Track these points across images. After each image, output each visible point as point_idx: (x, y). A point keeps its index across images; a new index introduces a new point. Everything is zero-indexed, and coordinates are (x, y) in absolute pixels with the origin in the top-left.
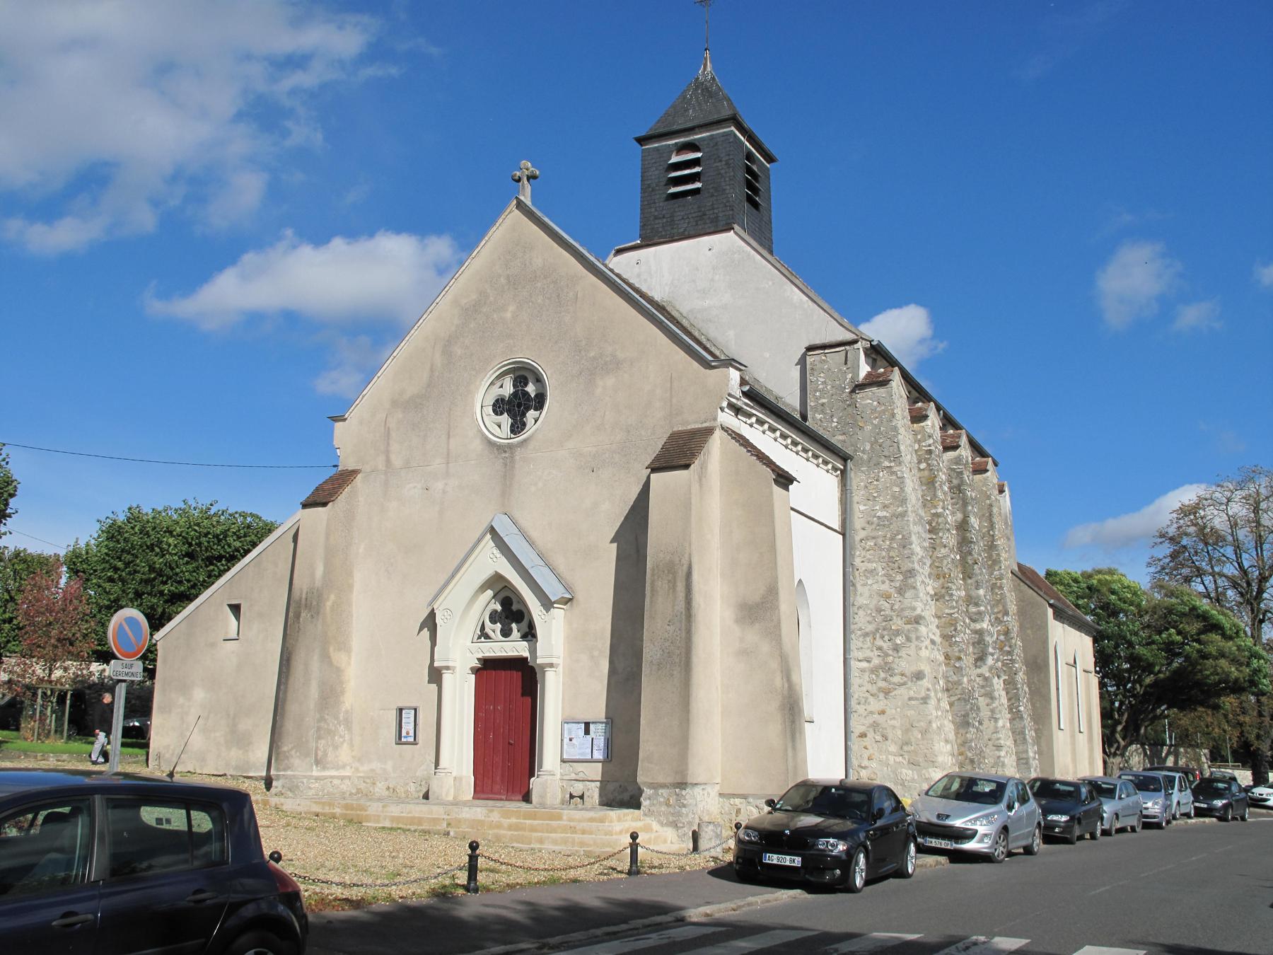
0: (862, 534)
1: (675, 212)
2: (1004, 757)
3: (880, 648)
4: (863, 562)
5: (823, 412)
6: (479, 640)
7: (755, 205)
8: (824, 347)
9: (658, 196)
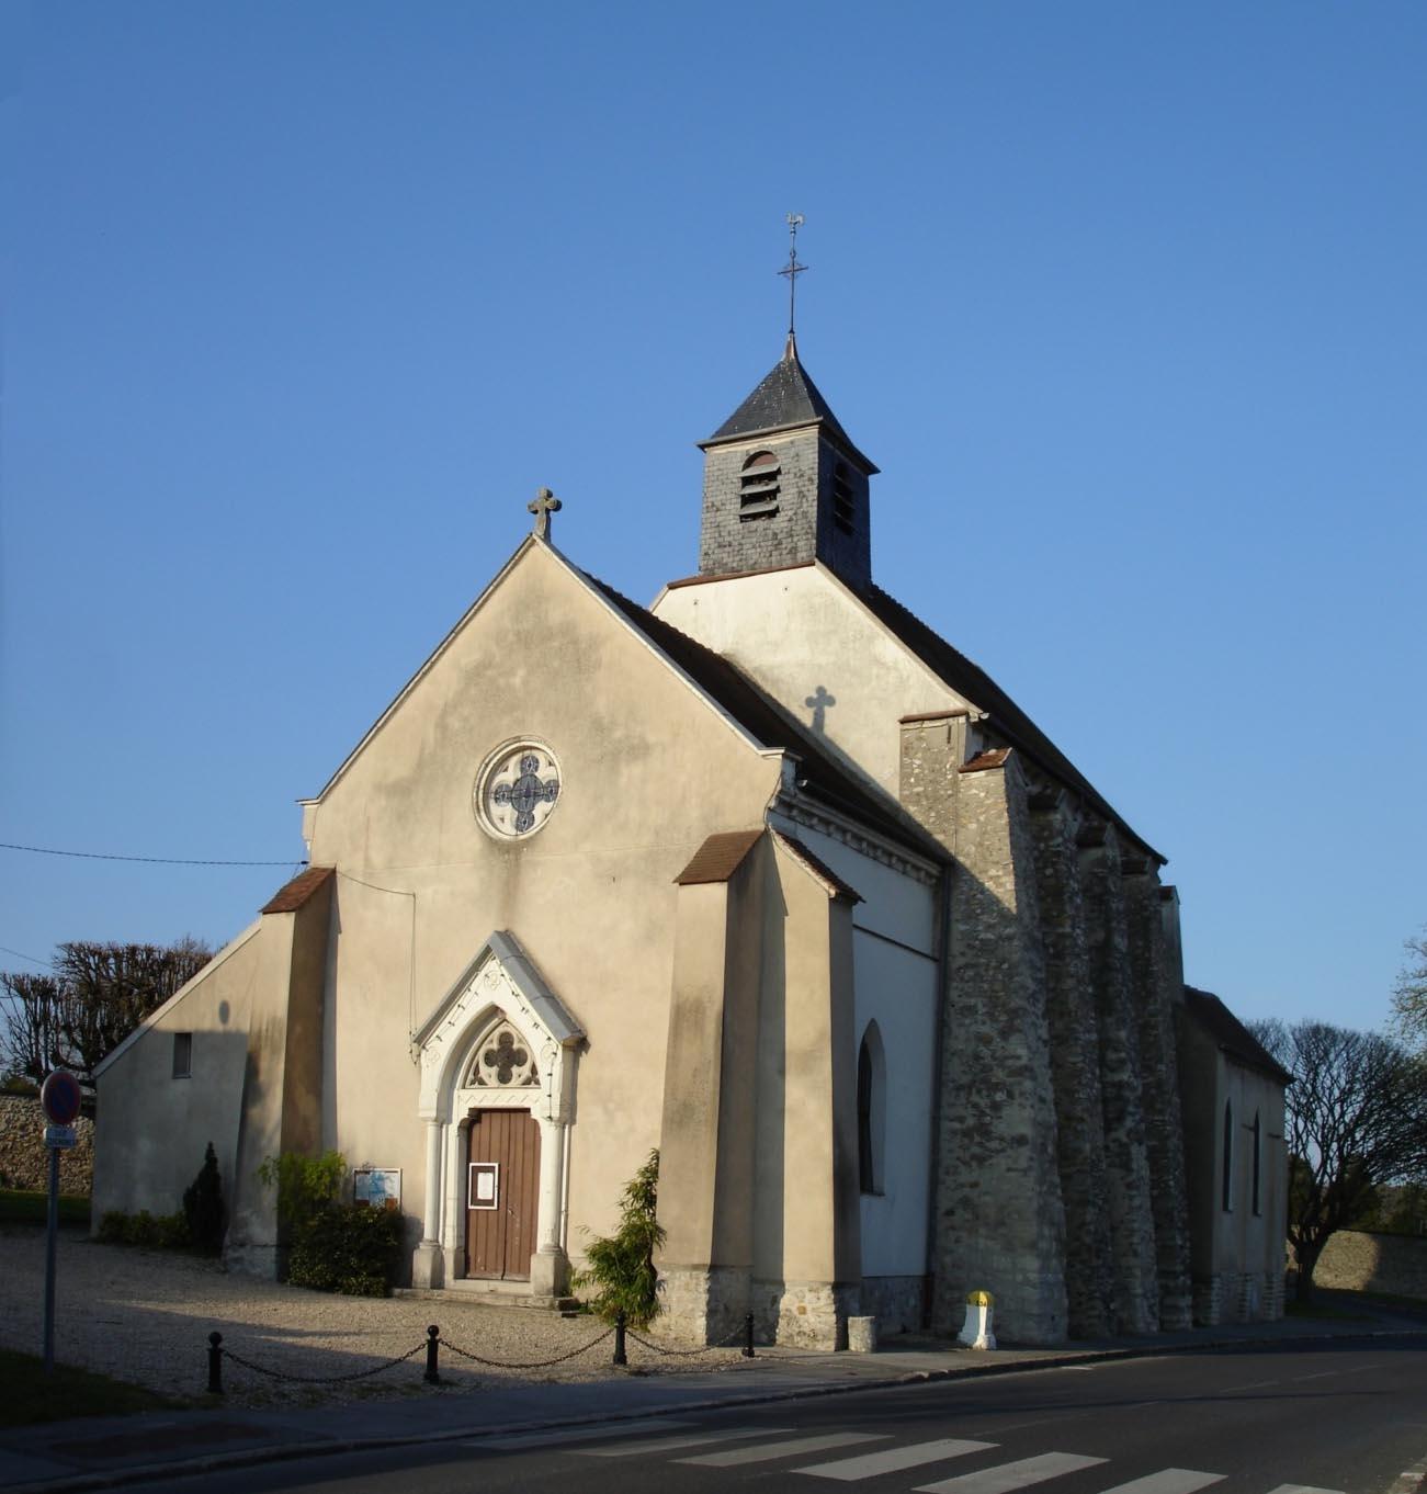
0: (960, 961)
2: (1138, 1244)
3: (975, 1106)
4: (960, 996)
7: (847, 530)
8: (922, 719)
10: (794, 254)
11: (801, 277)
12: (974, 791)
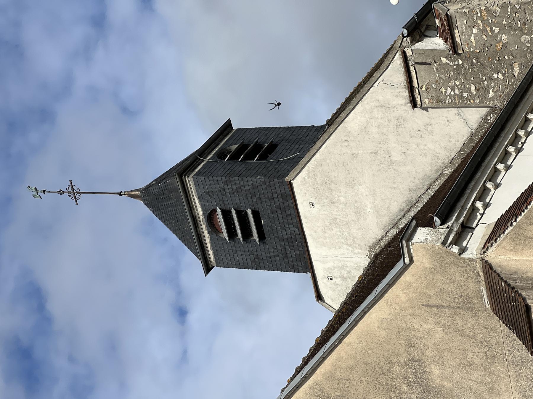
1: (278, 237)
5: (486, 90)
7: (273, 147)
9: (263, 253)
10: (61, 192)
11: (79, 186)
12: (472, 39)
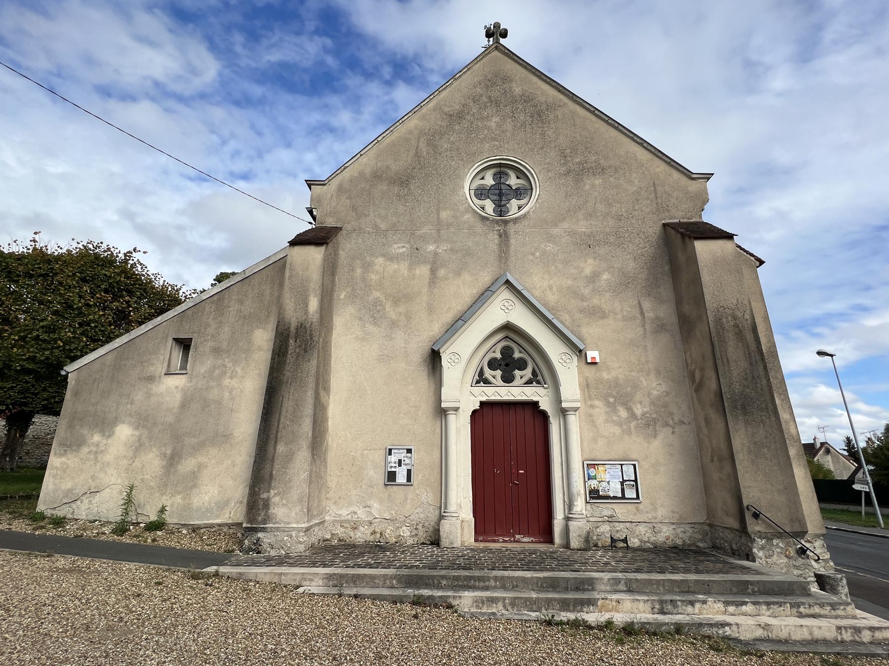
6: (476, 385)
